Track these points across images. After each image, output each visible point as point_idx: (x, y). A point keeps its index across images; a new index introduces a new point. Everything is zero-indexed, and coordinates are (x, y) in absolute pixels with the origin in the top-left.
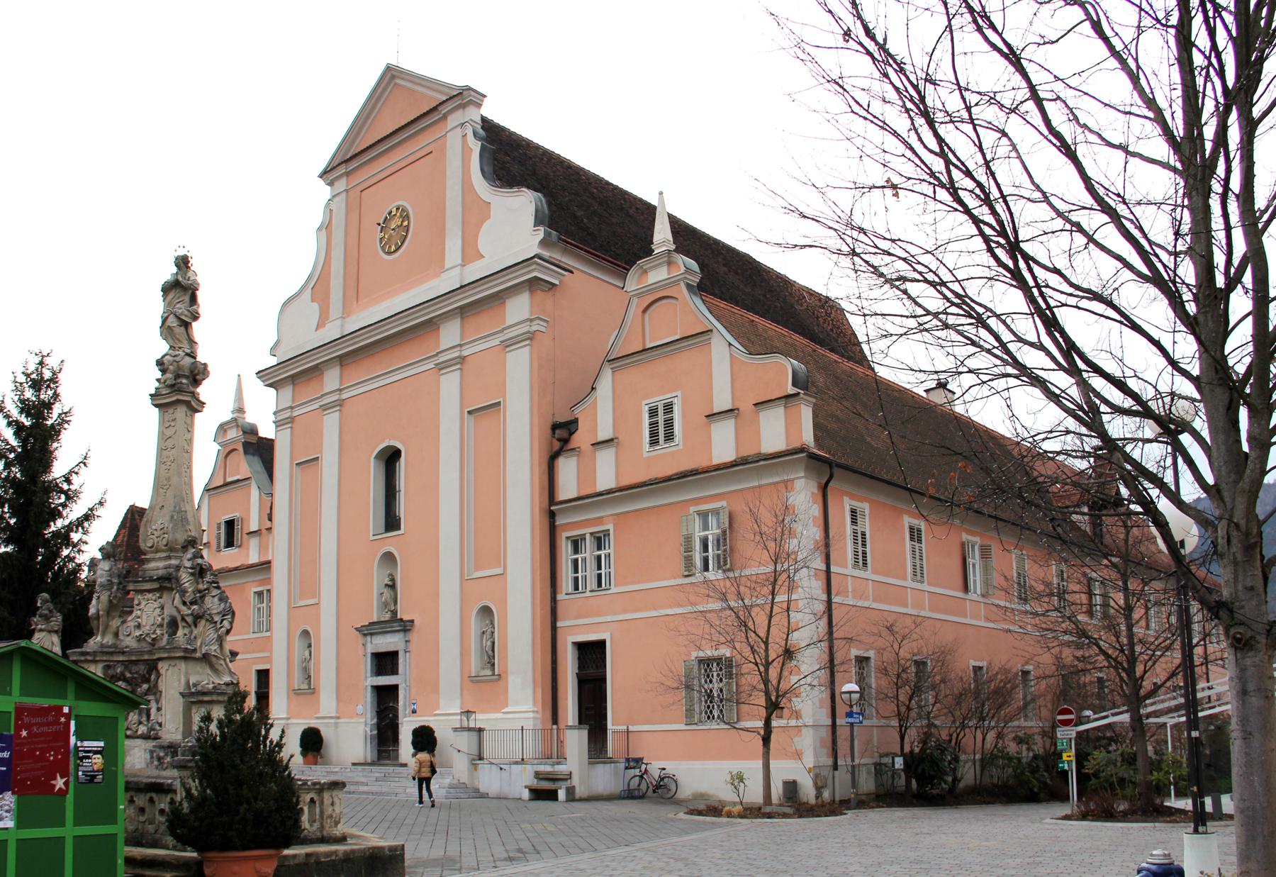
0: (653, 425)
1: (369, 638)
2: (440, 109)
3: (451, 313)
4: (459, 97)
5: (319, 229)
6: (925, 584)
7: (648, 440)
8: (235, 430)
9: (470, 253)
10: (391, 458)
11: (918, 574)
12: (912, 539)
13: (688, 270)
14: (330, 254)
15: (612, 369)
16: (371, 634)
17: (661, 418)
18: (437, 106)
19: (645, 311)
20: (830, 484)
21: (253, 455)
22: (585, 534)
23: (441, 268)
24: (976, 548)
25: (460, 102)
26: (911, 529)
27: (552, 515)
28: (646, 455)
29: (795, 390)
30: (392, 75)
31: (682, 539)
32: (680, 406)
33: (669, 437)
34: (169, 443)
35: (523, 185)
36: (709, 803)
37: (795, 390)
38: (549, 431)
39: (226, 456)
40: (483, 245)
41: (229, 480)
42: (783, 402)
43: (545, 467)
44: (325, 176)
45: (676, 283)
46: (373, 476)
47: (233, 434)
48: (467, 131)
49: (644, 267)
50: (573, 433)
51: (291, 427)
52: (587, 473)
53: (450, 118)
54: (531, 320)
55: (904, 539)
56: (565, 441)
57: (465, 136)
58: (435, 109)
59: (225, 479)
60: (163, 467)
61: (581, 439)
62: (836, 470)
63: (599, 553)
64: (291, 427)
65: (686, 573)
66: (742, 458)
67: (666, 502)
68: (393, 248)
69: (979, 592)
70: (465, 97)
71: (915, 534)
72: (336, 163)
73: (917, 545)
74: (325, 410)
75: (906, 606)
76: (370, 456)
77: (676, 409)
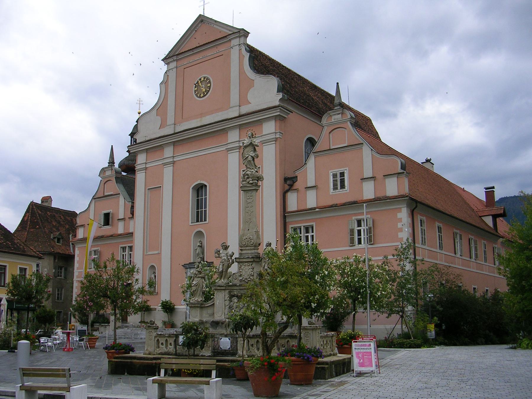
0: (335, 182)
1: (189, 270)
2: (228, 37)
3: (235, 127)
4: (238, 33)
5: (161, 83)
6: (443, 251)
7: (332, 187)
8: (110, 171)
9: (243, 100)
10: (200, 189)
11: (441, 247)
12: (439, 232)
13: (352, 117)
14: (167, 95)
15: (314, 156)
16: (190, 268)
17: (339, 179)
18: (227, 36)
19: (330, 133)
20: (415, 210)
21: (120, 183)
22: (301, 226)
23: (227, 106)
24: (458, 235)
25: (238, 35)
26: (438, 227)
27: (285, 217)
28: (331, 194)
29: (402, 171)
30: (202, 20)
31: (349, 231)
32: (348, 174)
33: (343, 186)
34: (250, 205)
35: (271, 74)
36: (110, 391)
37: (402, 171)
38: (283, 181)
39: (105, 184)
40: (250, 97)
41: (106, 194)
42: (397, 175)
43: (282, 196)
44: (165, 60)
45: (346, 122)
46: (190, 197)
47: (108, 173)
48: (241, 48)
49: (331, 114)
50: (295, 182)
51: (145, 172)
52: (302, 199)
53: (232, 41)
54: (276, 133)
55: (436, 232)
56: (291, 186)
57: (240, 50)
58: (226, 37)
59: (104, 194)
60: (247, 214)
61: (298, 185)
62: (418, 204)
63: (307, 234)
64: (173, 166)
65: (351, 245)
66: (378, 197)
67: (342, 214)
68: (202, 95)
69: (459, 254)
70: (244, 33)
71: (440, 229)
72: (171, 56)
73: (440, 234)
74: (164, 165)
75: (437, 260)
76: (190, 187)
77: (346, 175)
